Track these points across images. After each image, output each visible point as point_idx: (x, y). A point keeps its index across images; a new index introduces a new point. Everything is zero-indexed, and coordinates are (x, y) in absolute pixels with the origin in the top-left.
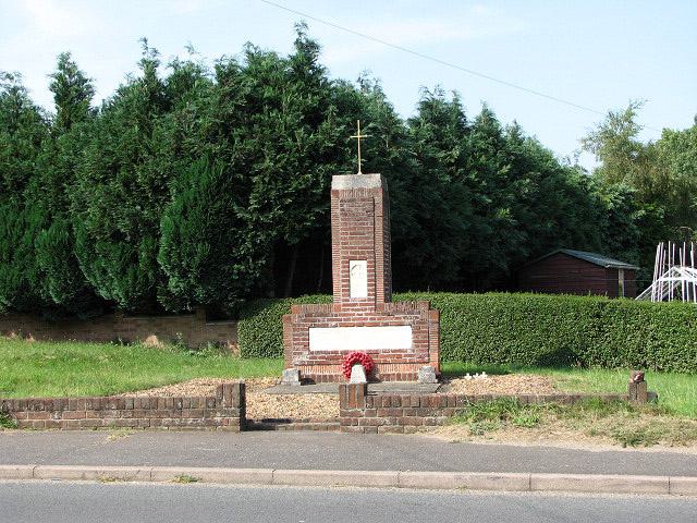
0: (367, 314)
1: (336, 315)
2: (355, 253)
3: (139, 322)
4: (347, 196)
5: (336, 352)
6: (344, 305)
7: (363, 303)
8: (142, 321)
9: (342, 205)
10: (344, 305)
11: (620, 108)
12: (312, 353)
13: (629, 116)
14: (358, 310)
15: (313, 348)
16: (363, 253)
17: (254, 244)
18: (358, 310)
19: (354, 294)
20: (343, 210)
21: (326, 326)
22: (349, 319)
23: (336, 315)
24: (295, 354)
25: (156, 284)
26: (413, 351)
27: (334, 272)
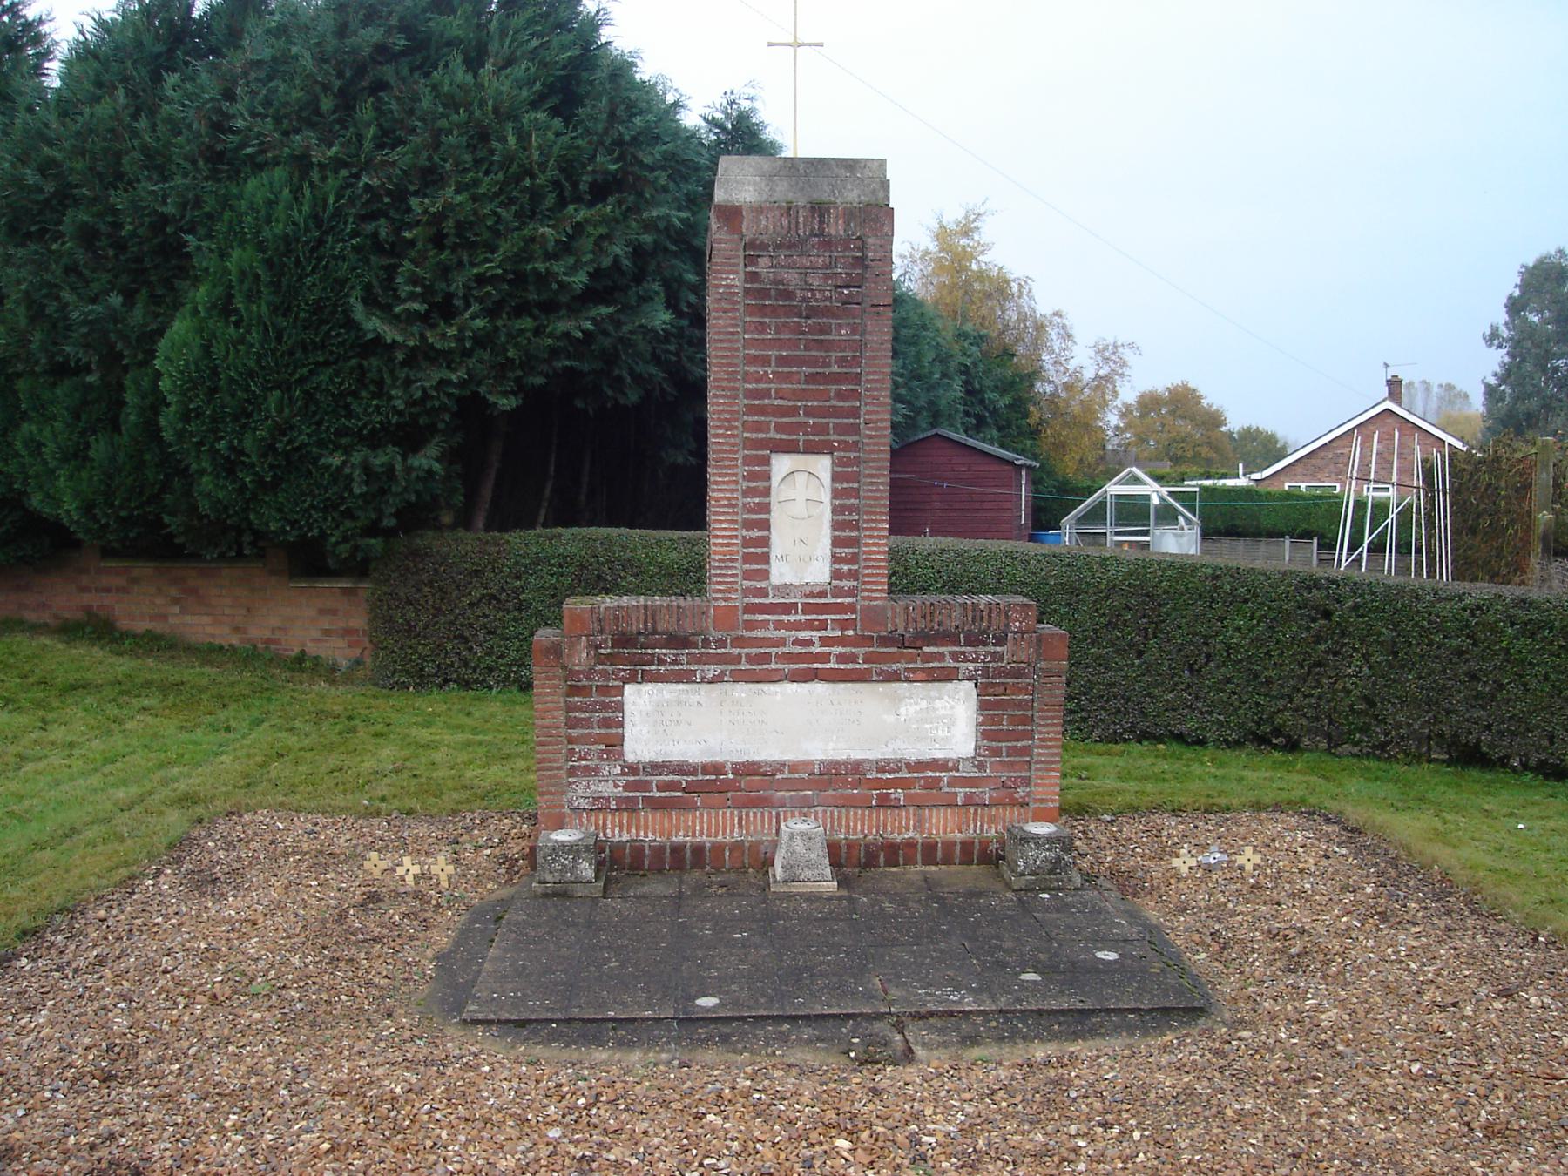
0: (825, 641)
1: (721, 643)
2: (792, 428)
3: (136, 573)
4: (767, 227)
5: (716, 768)
6: (749, 609)
7: (817, 603)
8: (143, 569)
9: (750, 260)
10: (749, 609)
11: (953, 216)
12: (633, 769)
13: (967, 231)
14: (798, 626)
15: (630, 757)
16: (824, 430)
17: (1496, 622)
18: (798, 626)
19: (782, 572)
20: (753, 277)
21: (684, 677)
22: (765, 658)
23: (721, 643)
24: (572, 772)
25: (165, 487)
26: (981, 766)
27: (713, 493)
